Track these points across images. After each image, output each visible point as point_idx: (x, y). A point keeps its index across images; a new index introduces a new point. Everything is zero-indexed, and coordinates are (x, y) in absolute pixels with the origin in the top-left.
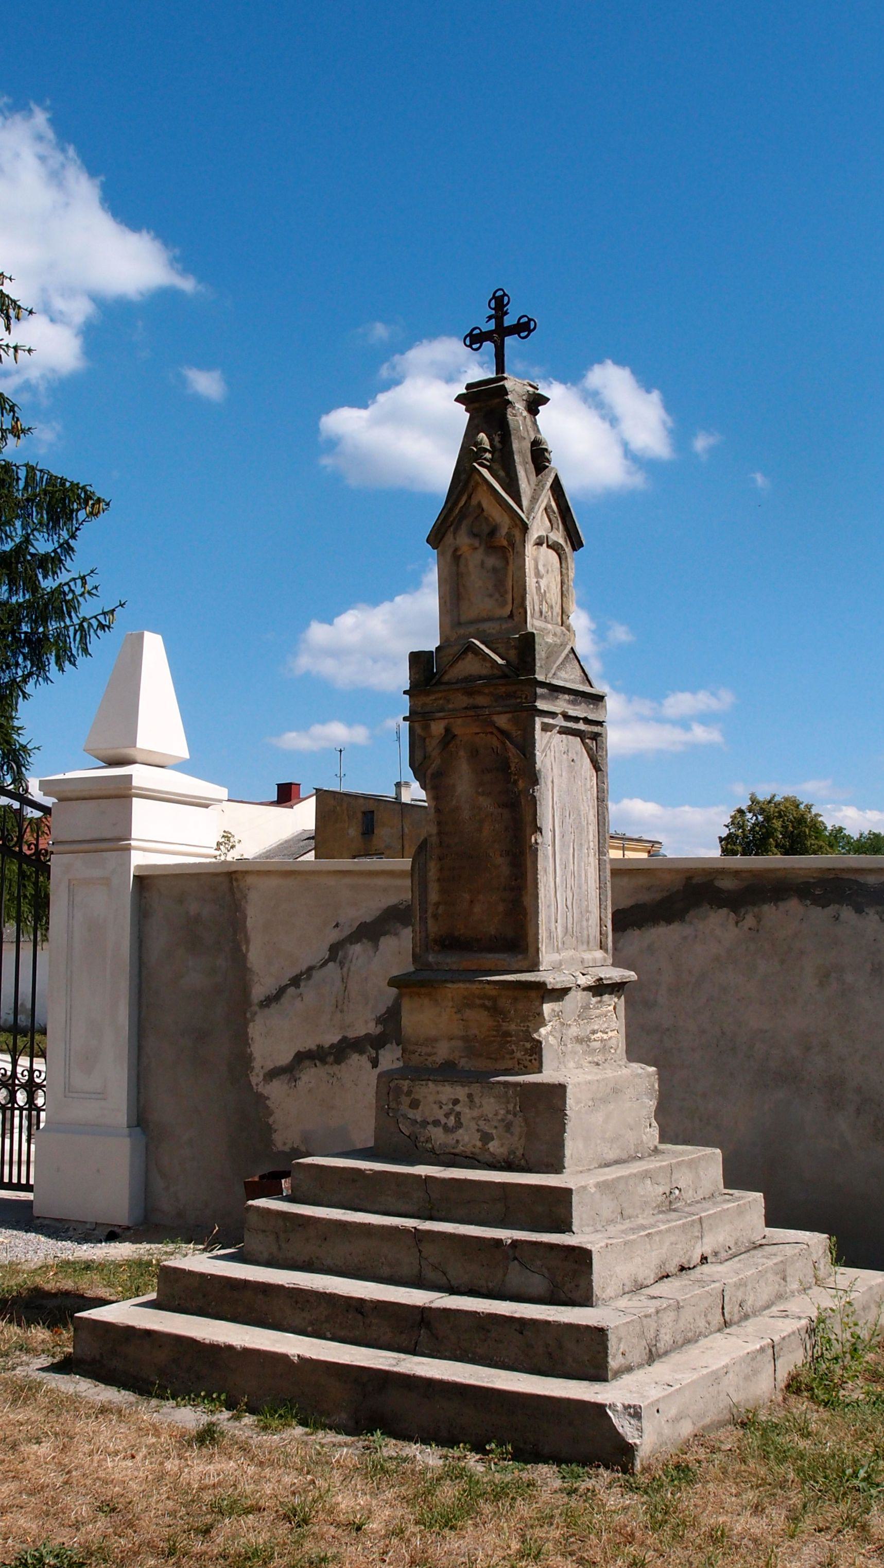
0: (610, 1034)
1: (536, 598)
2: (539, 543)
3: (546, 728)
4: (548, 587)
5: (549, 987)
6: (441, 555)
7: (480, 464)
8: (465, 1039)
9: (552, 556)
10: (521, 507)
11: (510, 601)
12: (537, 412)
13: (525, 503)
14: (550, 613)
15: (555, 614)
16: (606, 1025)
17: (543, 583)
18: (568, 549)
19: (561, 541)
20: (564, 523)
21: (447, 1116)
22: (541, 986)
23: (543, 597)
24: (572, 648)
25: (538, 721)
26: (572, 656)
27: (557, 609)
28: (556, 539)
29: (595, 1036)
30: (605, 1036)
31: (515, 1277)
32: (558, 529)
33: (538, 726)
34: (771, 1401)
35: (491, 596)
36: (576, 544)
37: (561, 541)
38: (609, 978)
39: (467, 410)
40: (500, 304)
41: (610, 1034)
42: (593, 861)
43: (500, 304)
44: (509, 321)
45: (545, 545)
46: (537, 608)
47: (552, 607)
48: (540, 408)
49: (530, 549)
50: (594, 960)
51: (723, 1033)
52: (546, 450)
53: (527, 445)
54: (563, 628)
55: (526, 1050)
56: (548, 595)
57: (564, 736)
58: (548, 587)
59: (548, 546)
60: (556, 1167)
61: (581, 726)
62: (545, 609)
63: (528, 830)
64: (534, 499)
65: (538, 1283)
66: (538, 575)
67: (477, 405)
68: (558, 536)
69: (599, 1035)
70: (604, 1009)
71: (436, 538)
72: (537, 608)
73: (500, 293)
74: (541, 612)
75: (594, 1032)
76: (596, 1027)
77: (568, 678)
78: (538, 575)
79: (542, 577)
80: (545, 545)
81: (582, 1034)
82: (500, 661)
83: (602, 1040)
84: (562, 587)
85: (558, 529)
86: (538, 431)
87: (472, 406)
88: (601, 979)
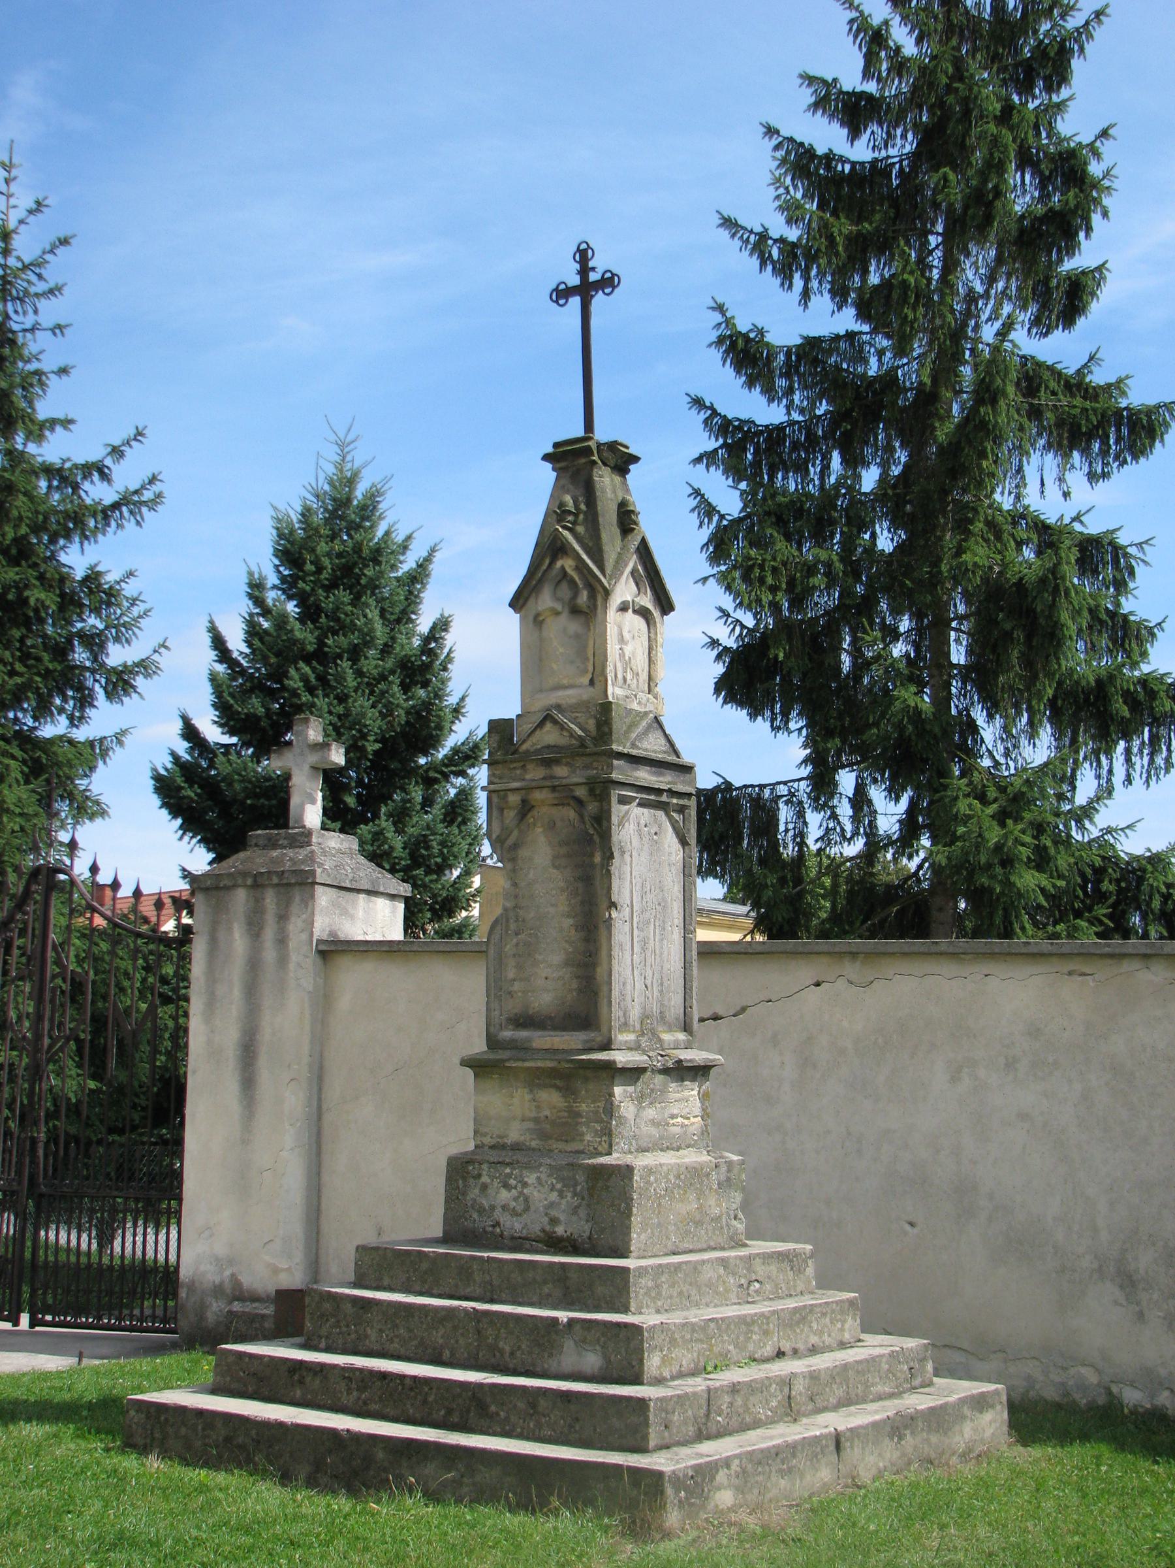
0: (692, 1120)
1: (619, 665)
2: (623, 608)
3: (623, 801)
4: (633, 653)
5: (619, 1066)
6: (522, 621)
7: (563, 527)
8: (536, 1120)
9: (639, 622)
10: (603, 572)
11: (591, 658)
12: (627, 471)
13: (609, 565)
14: (635, 681)
15: (641, 680)
16: (687, 1110)
17: (628, 650)
18: (656, 614)
19: (650, 606)
20: (653, 588)
21: (515, 1199)
22: (609, 1066)
23: (627, 664)
24: (656, 718)
25: (615, 793)
26: (655, 725)
27: (644, 676)
28: (642, 604)
29: (675, 1121)
30: (686, 1122)
31: (569, 1358)
32: (646, 594)
33: (614, 800)
34: (1141, 1315)
35: (572, 662)
36: (666, 605)
37: (650, 606)
38: (690, 1061)
39: (554, 469)
40: (583, 256)
41: (692, 1120)
42: (676, 936)
43: (583, 256)
44: (593, 277)
45: (630, 611)
46: (620, 676)
47: (638, 674)
48: (631, 467)
49: (612, 615)
50: (677, 1041)
51: (849, 1134)
52: (633, 512)
53: (614, 507)
54: (650, 696)
55: (596, 1131)
56: (633, 661)
57: (646, 811)
58: (633, 653)
59: (634, 611)
60: (624, 1255)
61: (664, 798)
62: (629, 677)
63: (604, 905)
64: (620, 562)
65: (592, 1361)
66: (622, 640)
67: (562, 464)
68: (647, 601)
69: (679, 1120)
70: (686, 1093)
71: (518, 602)
72: (620, 676)
73: (584, 246)
74: (625, 680)
75: (673, 1117)
76: (675, 1112)
77: (653, 746)
78: (622, 640)
79: (626, 644)
80: (630, 611)
81: (658, 1117)
82: (580, 733)
83: (683, 1126)
84: (649, 653)
85: (646, 594)
86: (627, 491)
87: (558, 465)
88: (681, 1061)
